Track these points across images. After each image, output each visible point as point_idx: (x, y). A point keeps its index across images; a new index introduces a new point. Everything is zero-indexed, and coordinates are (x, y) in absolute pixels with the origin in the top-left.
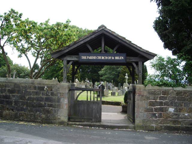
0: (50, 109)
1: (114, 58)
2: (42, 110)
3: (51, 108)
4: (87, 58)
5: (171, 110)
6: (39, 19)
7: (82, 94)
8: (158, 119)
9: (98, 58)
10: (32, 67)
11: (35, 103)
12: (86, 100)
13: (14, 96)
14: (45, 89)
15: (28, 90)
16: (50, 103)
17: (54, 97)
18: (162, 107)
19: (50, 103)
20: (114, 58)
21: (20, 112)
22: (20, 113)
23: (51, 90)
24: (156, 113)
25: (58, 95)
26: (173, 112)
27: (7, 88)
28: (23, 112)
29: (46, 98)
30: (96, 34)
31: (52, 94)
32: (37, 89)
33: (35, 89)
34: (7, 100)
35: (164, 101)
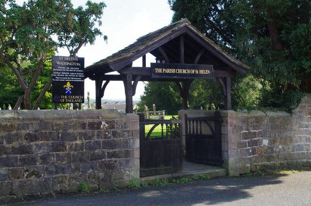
0: (112, 161)
1: (199, 72)
2: (98, 164)
3: (113, 159)
4: (162, 70)
5: (265, 142)
6: (53, 40)
7: (156, 128)
8: (252, 156)
9: (178, 71)
10: (153, 125)
11: (35, 67)
12: (161, 135)
13: (39, 147)
14: (102, 126)
15: (70, 131)
16: (111, 151)
17: (117, 139)
18: (256, 139)
19: (111, 151)
20: (199, 72)
21: (54, 176)
22: (55, 178)
23: (113, 127)
24: (249, 148)
25: (124, 135)
26: (267, 145)
27: (24, 132)
28: (61, 174)
29: (104, 142)
30: (176, 34)
31: (115, 134)
32: (87, 127)
33: (84, 128)
34: (24, 155)
35: (257, 131)
